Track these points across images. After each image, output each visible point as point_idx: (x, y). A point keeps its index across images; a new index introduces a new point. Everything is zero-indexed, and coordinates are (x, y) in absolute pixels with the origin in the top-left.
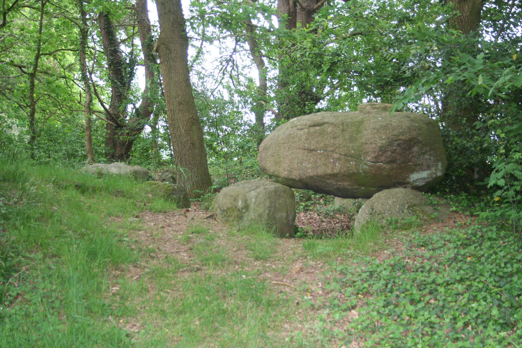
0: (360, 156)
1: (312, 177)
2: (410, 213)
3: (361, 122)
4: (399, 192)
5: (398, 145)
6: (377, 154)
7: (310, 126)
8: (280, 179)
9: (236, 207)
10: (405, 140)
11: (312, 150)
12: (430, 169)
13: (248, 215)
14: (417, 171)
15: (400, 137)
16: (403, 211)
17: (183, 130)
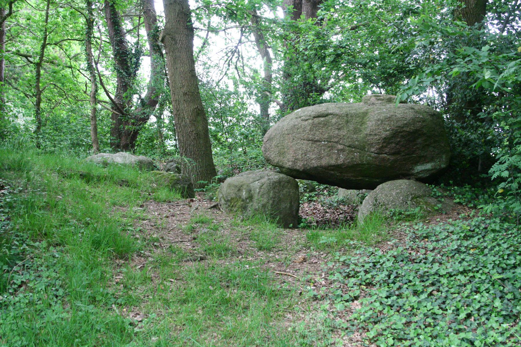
2: (413, 204)
7: (314, 117)
15: (405, 129)
16: (406, 203)
17: (188, 120)
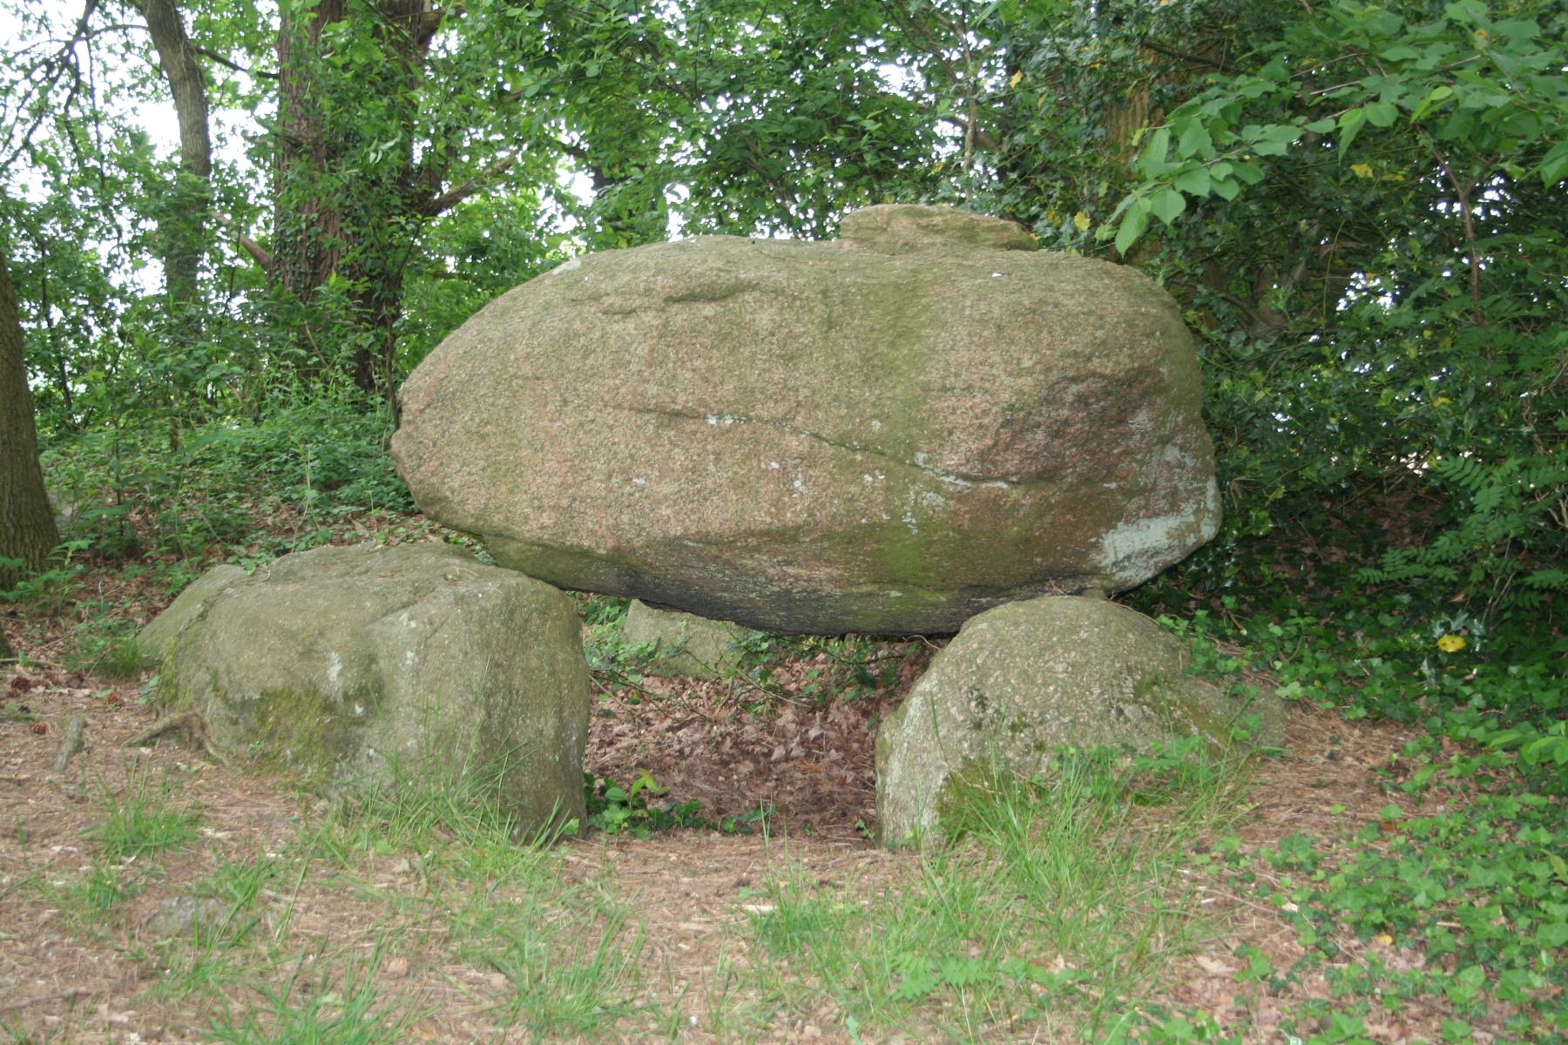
0: (912, 449)
1: (673, 544)
2: (1148, 719)
3: (909, 291)
4: (1058, 606)
5: (1082, 400)
6: (989, 442)
7: (671, 300)
8: (512, 549)
9: (313, 690)
10: (1112, 379)
11: (678, 414)
12: (1179, 511)
13: (383, 734)
14: (1131, 519)
15: (1095, 364)
16: (1120, 712)
